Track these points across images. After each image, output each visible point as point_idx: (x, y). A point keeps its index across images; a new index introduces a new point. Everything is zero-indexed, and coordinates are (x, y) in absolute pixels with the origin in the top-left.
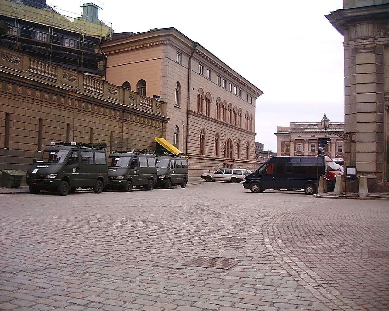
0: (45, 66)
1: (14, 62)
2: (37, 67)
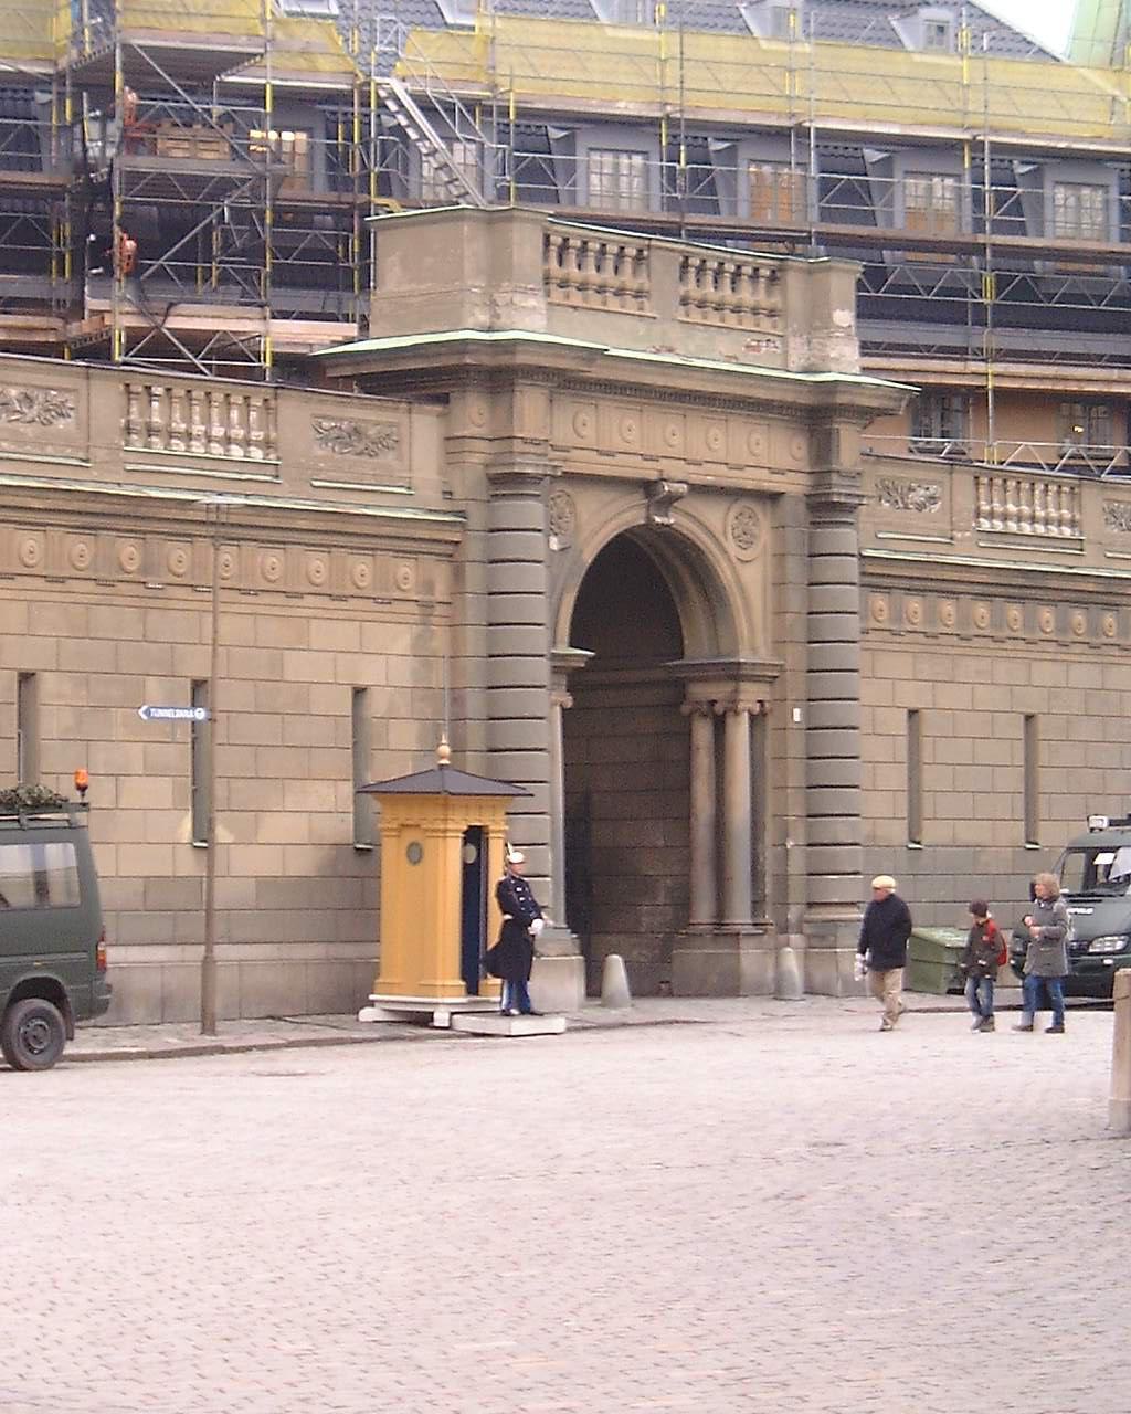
0: (1033, 491)
1: (920, 507)
2: (1004, 502)
